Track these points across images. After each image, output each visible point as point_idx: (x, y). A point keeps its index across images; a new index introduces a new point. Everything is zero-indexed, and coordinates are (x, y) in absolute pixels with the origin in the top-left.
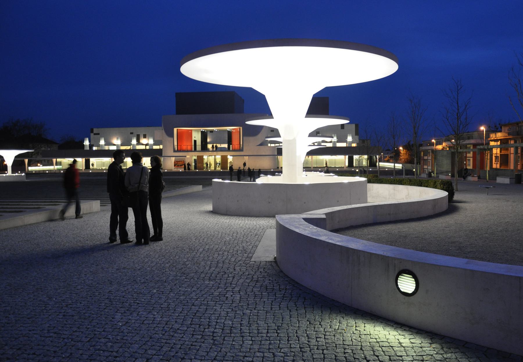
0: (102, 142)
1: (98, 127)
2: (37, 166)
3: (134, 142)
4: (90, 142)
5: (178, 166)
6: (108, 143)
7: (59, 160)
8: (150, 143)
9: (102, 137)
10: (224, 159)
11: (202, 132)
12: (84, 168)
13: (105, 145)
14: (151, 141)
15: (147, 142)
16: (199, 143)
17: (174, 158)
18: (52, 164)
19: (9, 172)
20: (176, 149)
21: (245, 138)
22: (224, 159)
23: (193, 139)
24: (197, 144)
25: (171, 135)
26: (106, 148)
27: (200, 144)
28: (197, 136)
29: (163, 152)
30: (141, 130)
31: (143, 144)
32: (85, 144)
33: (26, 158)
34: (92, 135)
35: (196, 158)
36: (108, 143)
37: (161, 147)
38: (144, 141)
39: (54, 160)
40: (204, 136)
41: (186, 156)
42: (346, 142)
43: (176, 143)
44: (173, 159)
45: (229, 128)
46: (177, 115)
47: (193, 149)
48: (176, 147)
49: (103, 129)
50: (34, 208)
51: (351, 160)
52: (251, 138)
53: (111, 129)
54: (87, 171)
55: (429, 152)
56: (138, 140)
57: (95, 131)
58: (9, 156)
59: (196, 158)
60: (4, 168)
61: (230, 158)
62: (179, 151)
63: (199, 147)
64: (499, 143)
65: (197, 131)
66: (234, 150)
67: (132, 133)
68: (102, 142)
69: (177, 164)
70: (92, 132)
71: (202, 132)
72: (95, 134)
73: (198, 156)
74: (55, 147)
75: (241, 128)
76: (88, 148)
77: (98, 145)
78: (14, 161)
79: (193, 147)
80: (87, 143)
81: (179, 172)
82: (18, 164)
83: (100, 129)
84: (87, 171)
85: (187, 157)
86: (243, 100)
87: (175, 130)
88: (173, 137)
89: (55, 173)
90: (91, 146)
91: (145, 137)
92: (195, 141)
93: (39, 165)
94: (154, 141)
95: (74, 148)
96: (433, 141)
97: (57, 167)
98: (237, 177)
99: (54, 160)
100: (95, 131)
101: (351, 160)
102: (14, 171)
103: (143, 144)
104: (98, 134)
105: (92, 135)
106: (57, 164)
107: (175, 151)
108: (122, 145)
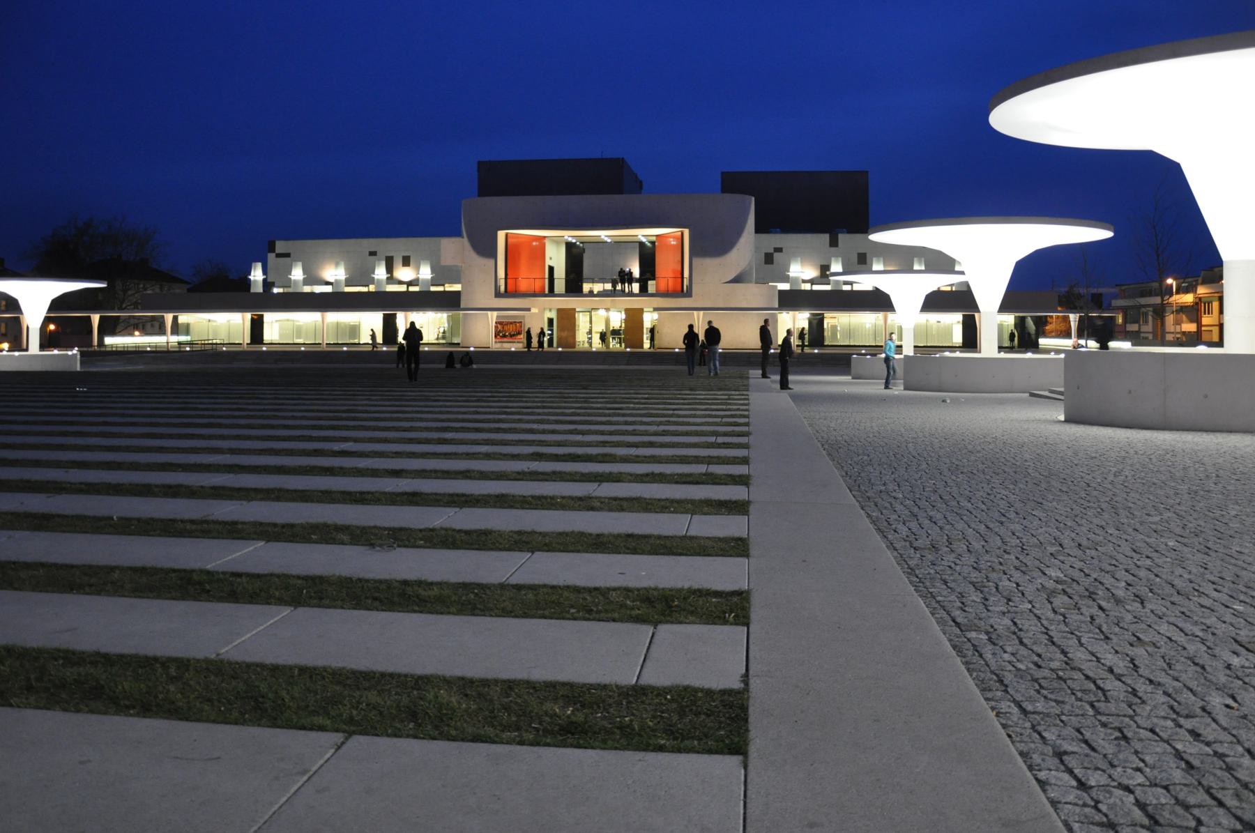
0: (297, 274)
1: (287, 238)
2: (132, 334)
3: (380, 273)
4: (265, 272)
5: (504, 336)
7: (184, 318)
10: (634, 318)
11: (569, 246)
12: (248, 340)
14: (425, 272)
16: (560, 273)
17: (495, 313)
18: (162, 331)
19: (34, 347)
20: (502, 289)
22: (634, 318)
23: (548, 262)
24: (556, 275)
25: (487, 250)
26: (307, 289)
27: (563, 275)
28: (556, 258)
29: (463, 298)
30: (397, 246)
31: (401, 283)
32: (251, 278)
33: (95, 309)
34: (271, 256)
35: (553, 315)
37: (457, 287)
38: (404, 273)
39: (169, 317)
40: (574, 255)
41: (529, 310)
43: (501, 273)
44: (493, 316)
45: (644, 234)
48: (502, 284)
49: (299, 243)
52: (710, 263)
54: (256, 348)
55: (1146, 314)
56: (390, 269)
57: (281, 246)
58: (35, 297)
59: (553, 315)
60: (14, 333)
61: (649, 319)
62: (508, 294)
63: (560, 286)
65: (556, 241)
67: (373, 254)
68: (297, 274)
69: (505, 330)
70: (272, 249)
71: (569, 246)
72: (279, 256)
73: (559, 311)
74: (179, 290)
75: (686, 232)
76: (261, 290)
77: (288, 283)
80: (257, 275)
82: (65, 323)
83: (291, 242)
84: (256, 348)
85: (534, 310)
87: (501, 235)
88: (494, 255)
89: (168, 352)
90: (267, 285)
91: (406, 262)
92: (551, 269)
95: (226, 290)
96: (1170, 281)
97: (174, 339)
98: (779, 369)
99: (169, 317)
100: (281, 246)
102: (48, 341)
103: (401, 283)
104: (288, 255)
105: (271, 256)
106: (176, 329)
107: (498, 294)
108: (349, 283)
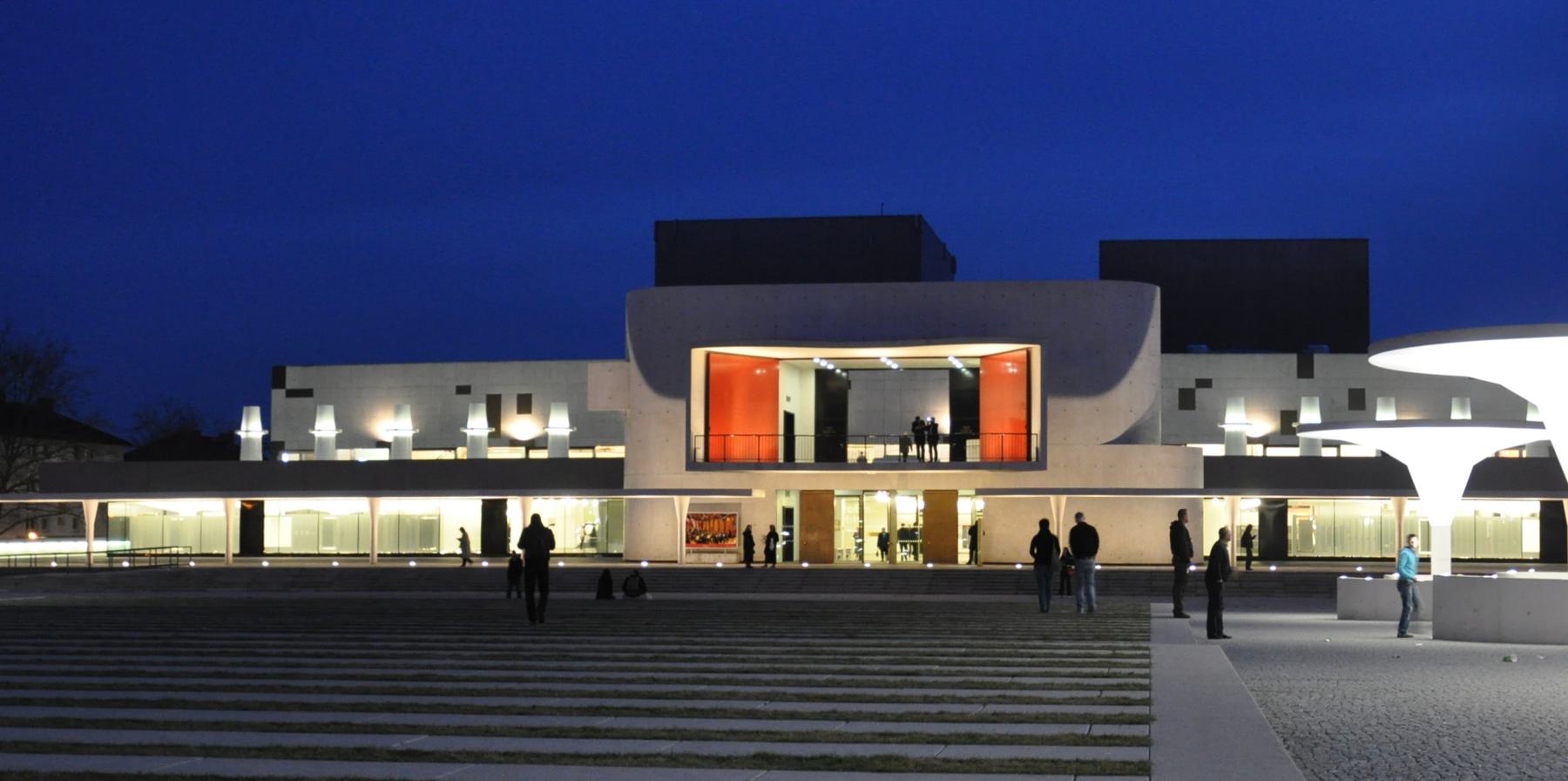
0: (325, 427)
1: (306, 362)
2: (23, 538)
3: (477, 425)
4: (266, 424)
5: (704, 541)
7: (119, 508)
8: (552, 432)
9: (325, 402)
10: (940, 507)
11: (822, 376)
14: (560, 424)
15: (541, 427)
16: (806, 425)
17: (687, 499)
18: (76, 530)
20: (700, 454)
21: (1053, 403)
22: (940, 507)
23: (784, 406)
24: (798, 430)
26: (343, 455)
27: (811, 430)
28: (798, 397)
30: (506, 376)
31: (514, 443)
32: (242, 434)
34: (278, 395)
35: (793, 502)
36: (352, 436)
37: (617, 452)
38: (520, 426)
39: (91, 507)
41: (748, 492)
42: (462, 440)
44: (683, 504)
45: (959, 354)
46: (1111, 285)
47: (781, 460)
48: (699, 444)
50: (509, 757)
51: (494, 519)
53: (370, 368)
54: (249, 562)
56: (494, 419)
57: (295, 376)
59: (793, 502)
61: (968, 509)
62: (711, 463)
63: (805, 448)
64: (853, 451)
65: (798, 366)
66: (984, 464)
67: (463, 390)
68: (325, 427)
70: (279, 381)
71: (822, 376)
72: (292, 394)
74: (109, 456)
75: (1036, 350)
76: (256, 455)
77: (308, 444)
79: (781, 440)
80: (252, 429)
81: (711, 572)
83: (313, 369)
84: (249, 562)
85: (758, 494)
90: (271, 447)
91: (524, 405)
92: (789, 418)
93: (32, 535)
94: (573, 421)
95: (199, 459)
97: (101, 547)
98: (1205, 600)
99: (91, 507)
100: (295, 376)
101: (252, 522)
103: (514, 443)
104: (308, 393)
105: (278, 395)
106: (105, 527)
107: (692, 465)
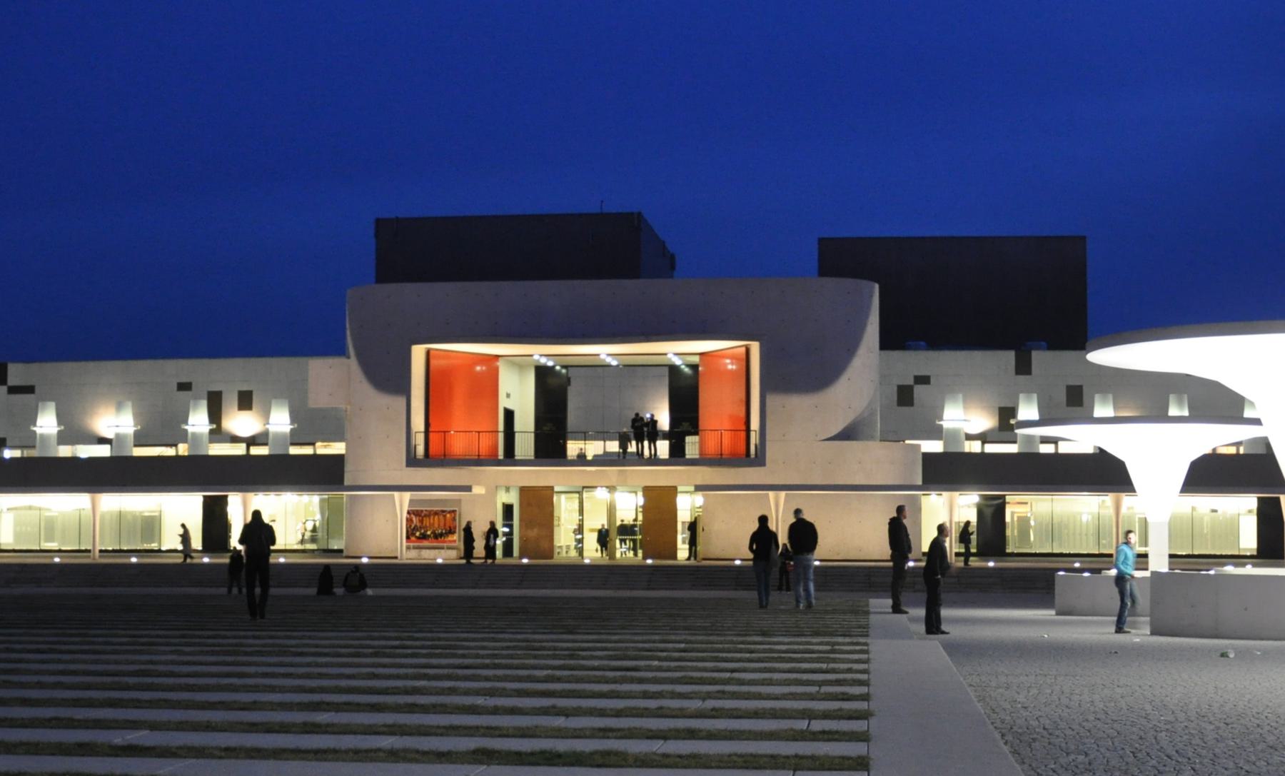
0: (47, 423)
3: (198, 422)
5: (424, 537)
6: (73, 433)
10: (659, 504)
11: (543, 374)
13: (63, 438)
14: (280, 421)
15: (263, 424)
16: (525, 422)
17: (407, 496)
20: (420, 450)
21: (772, 400)
22: (659, 504)
23: (504, 403)
24: (517, 427)
25: (395, 382)
26: (65, 451)
28: (518, 394)
30: (227, 373)
31: (235, 439)
35: (512, 498)
37: (338, 448)
38: (241, 423)
40: (551, 391)
41: (468, 489)
43: (418, 423)
44: (403, 501)
45: (679, 351)
52: (798, 404)
56: (215, 415)
59: (512, 498)
61: (687, 505)
62: (430, 460)
63: (525, 445)
65: (518, 363)
66: (703, 461)
67: (184, 387)
68: (47, 423)
71: (543, 374)
72: (13, 390)
75: (755, 347)
77: (29, 440)
78: (632, 214)
79: (501, 437)
85: (478, 490)
86: (672, 257)
88: (402, 388)
91: (245, 402)
92: (509, 415)
100: (16, 373)
103: (235, 439)
104: (29, 390)
107: (412, 461)
